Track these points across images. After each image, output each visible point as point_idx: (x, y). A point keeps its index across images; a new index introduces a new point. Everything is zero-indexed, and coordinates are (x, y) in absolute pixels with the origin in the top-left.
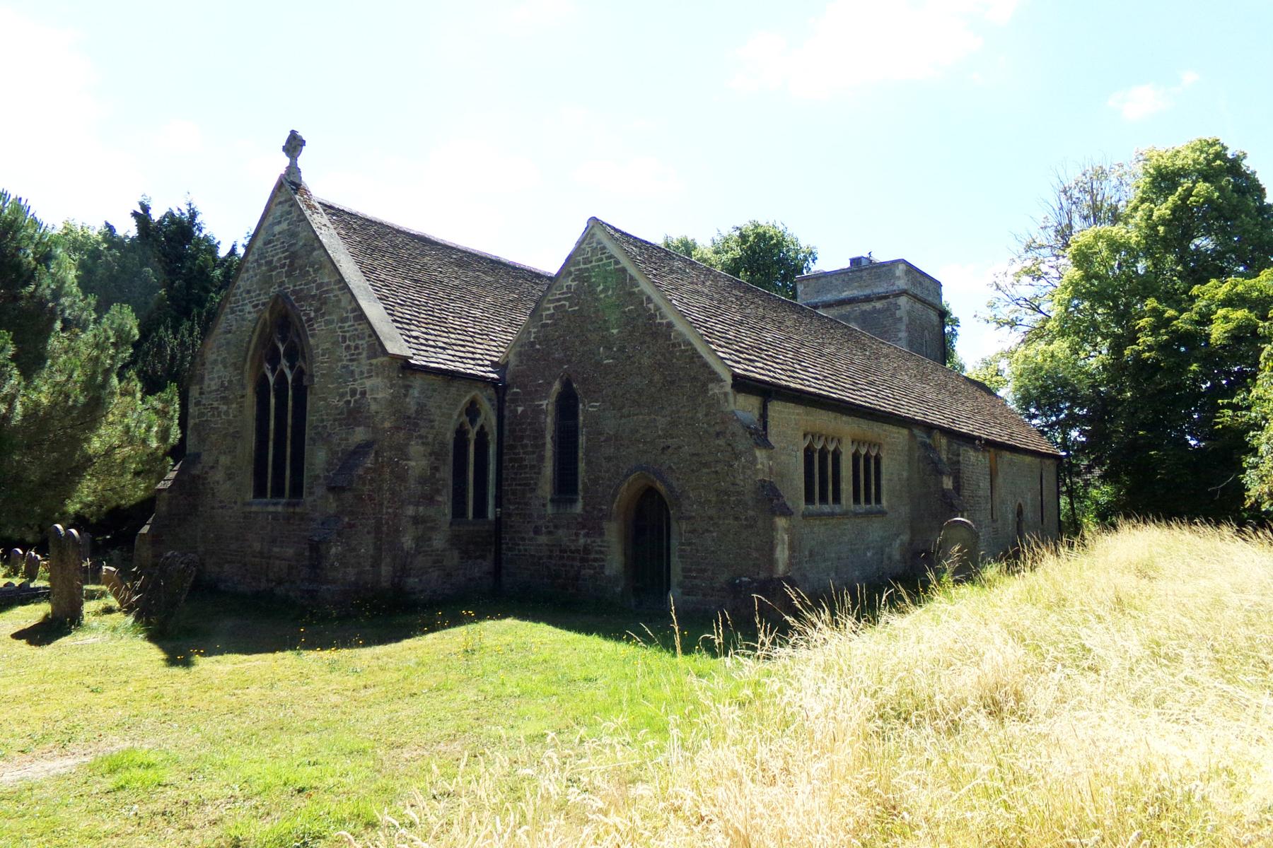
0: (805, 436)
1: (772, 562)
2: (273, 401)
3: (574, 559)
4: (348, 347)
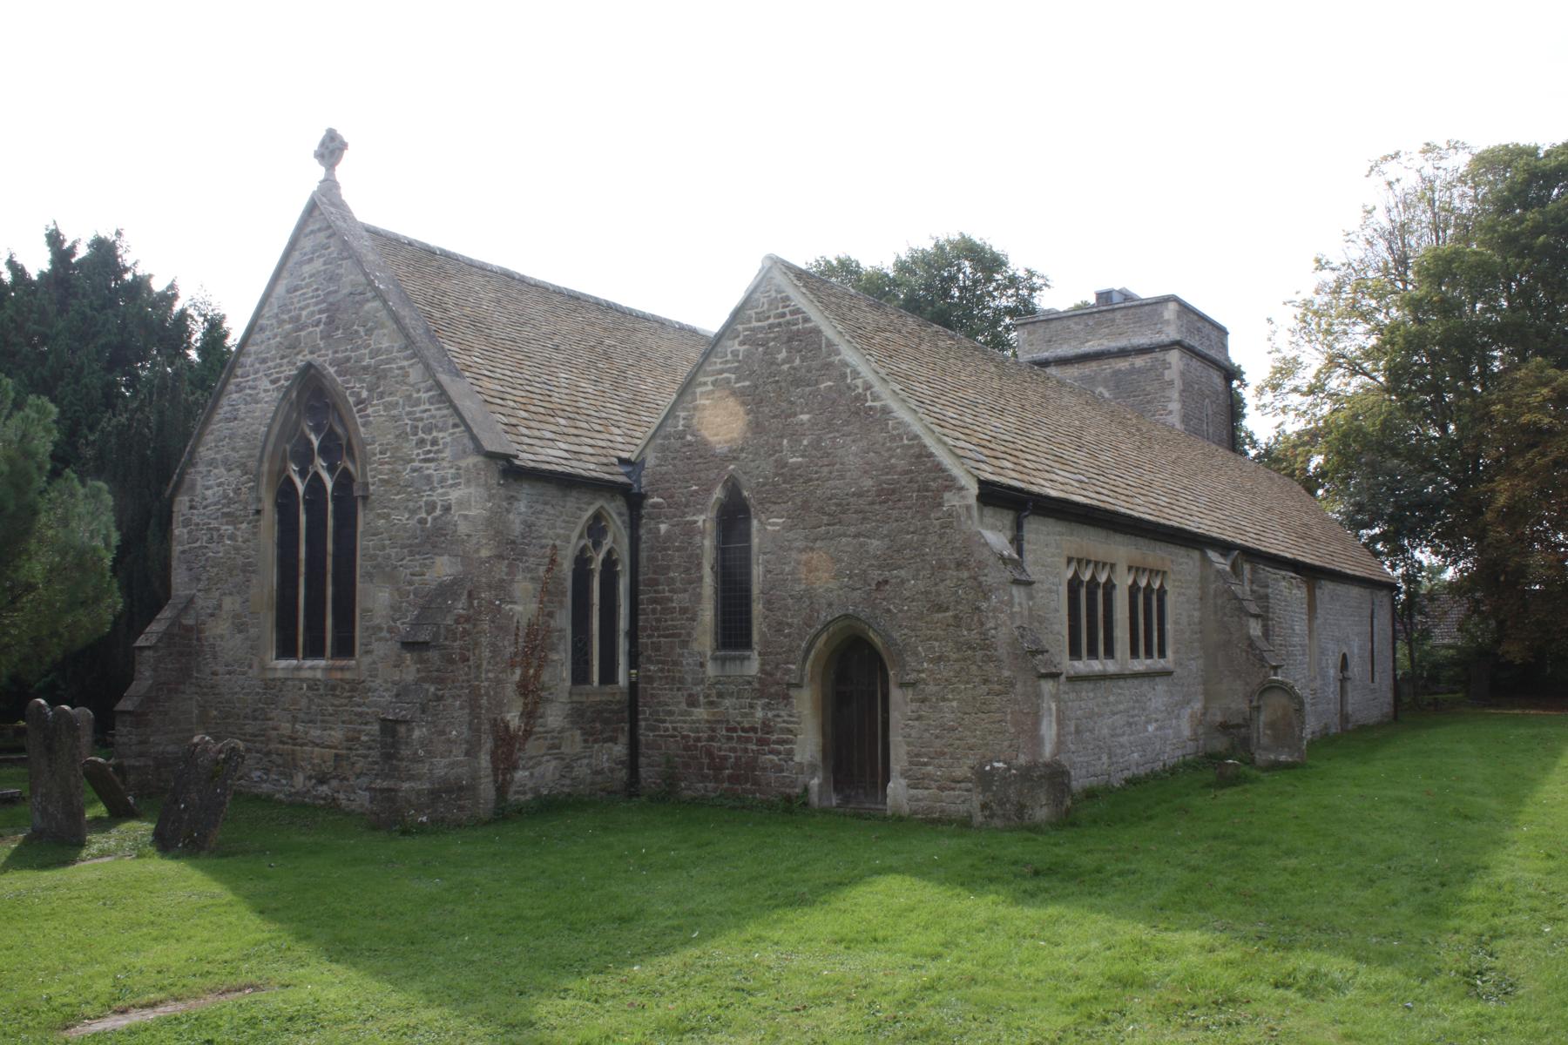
0: (1070, 560)
1: (1037, 740)
2: (303, 518)
3: (748, 740)
4: (422, 442)
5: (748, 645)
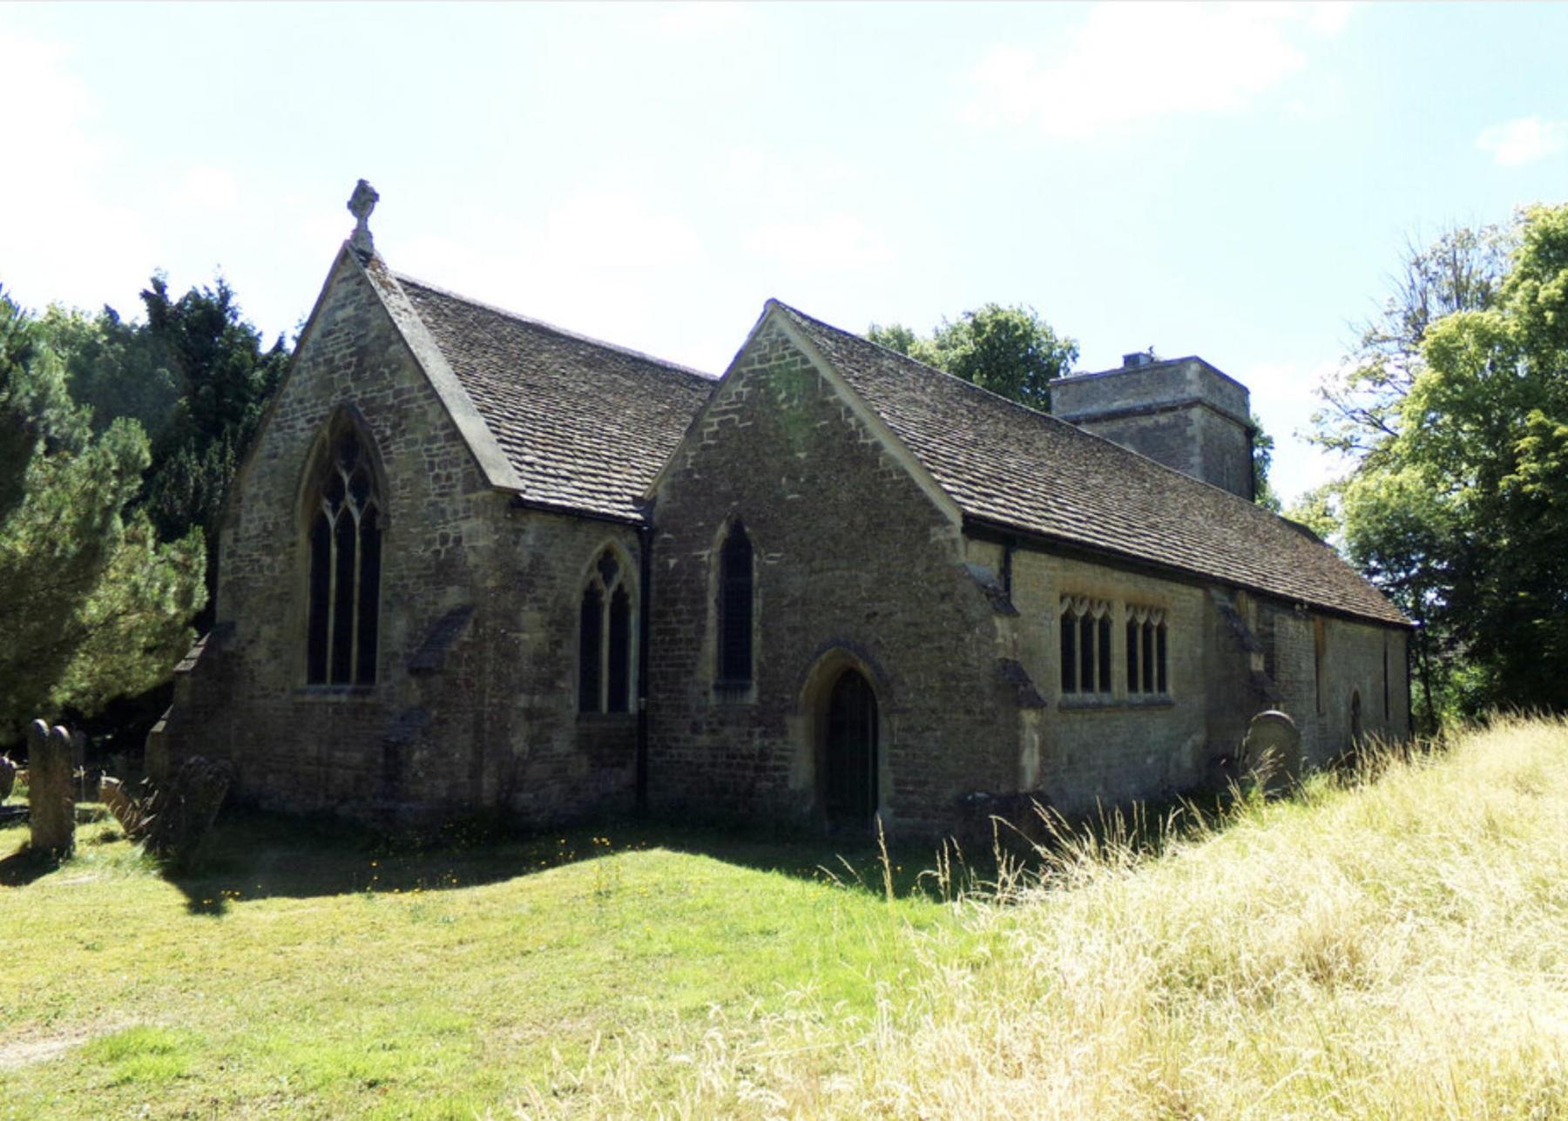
1: (1016, 771)
4: (437, 477)
5: (748, 674)
